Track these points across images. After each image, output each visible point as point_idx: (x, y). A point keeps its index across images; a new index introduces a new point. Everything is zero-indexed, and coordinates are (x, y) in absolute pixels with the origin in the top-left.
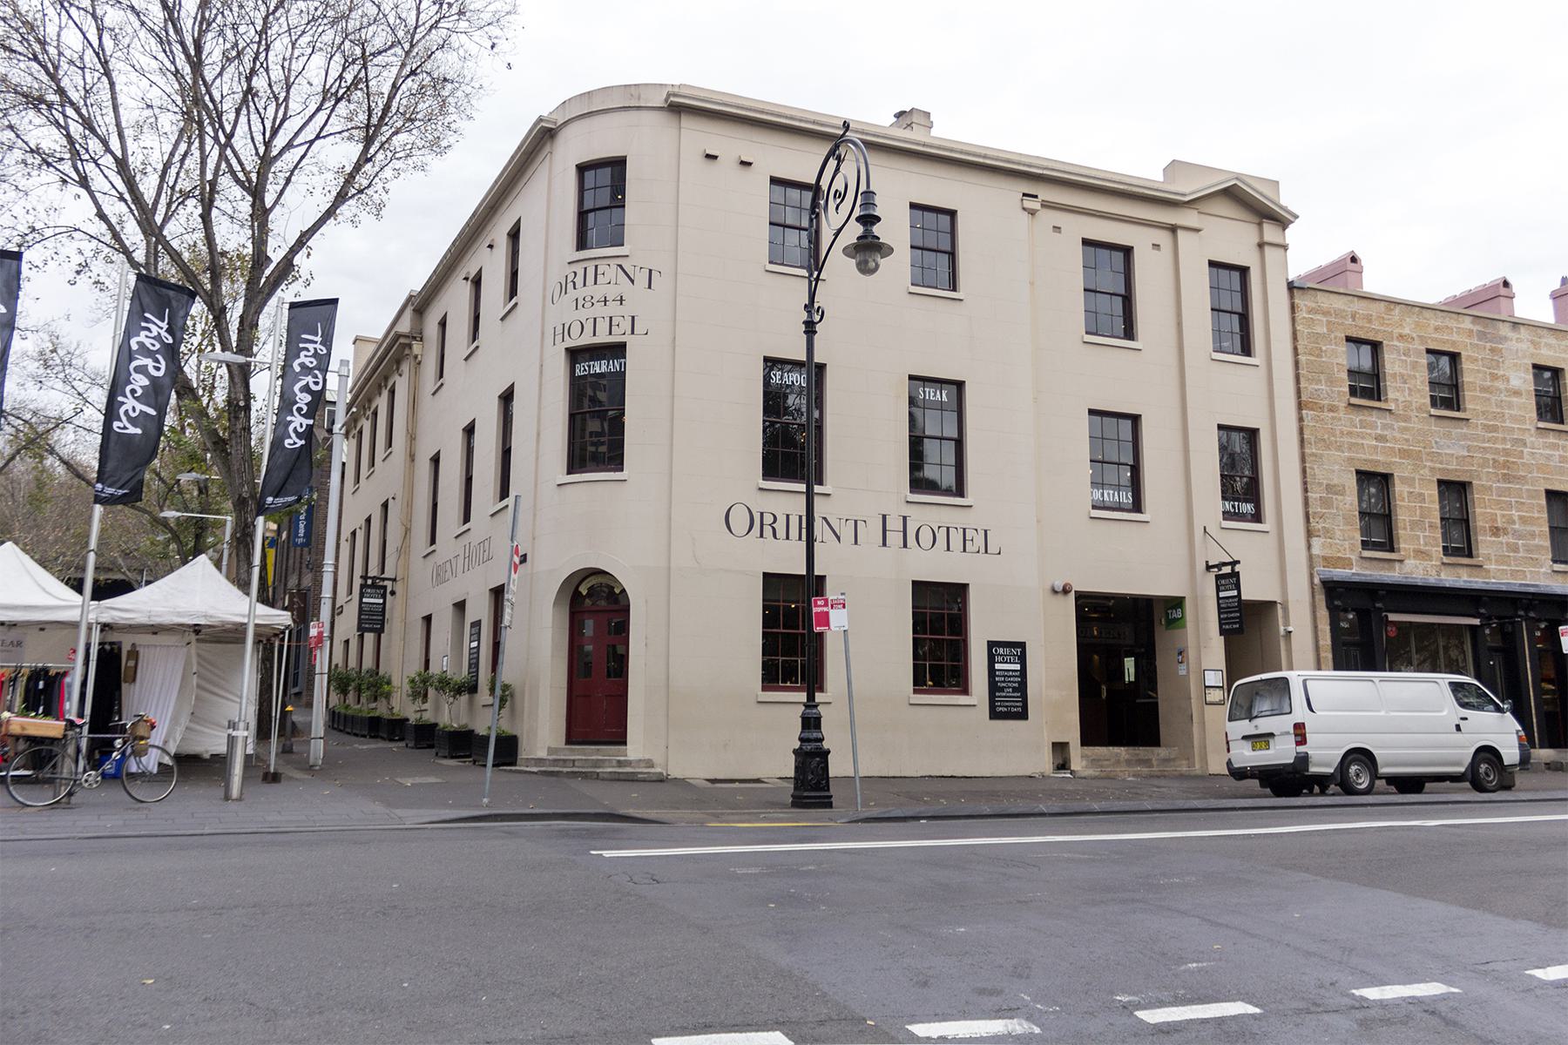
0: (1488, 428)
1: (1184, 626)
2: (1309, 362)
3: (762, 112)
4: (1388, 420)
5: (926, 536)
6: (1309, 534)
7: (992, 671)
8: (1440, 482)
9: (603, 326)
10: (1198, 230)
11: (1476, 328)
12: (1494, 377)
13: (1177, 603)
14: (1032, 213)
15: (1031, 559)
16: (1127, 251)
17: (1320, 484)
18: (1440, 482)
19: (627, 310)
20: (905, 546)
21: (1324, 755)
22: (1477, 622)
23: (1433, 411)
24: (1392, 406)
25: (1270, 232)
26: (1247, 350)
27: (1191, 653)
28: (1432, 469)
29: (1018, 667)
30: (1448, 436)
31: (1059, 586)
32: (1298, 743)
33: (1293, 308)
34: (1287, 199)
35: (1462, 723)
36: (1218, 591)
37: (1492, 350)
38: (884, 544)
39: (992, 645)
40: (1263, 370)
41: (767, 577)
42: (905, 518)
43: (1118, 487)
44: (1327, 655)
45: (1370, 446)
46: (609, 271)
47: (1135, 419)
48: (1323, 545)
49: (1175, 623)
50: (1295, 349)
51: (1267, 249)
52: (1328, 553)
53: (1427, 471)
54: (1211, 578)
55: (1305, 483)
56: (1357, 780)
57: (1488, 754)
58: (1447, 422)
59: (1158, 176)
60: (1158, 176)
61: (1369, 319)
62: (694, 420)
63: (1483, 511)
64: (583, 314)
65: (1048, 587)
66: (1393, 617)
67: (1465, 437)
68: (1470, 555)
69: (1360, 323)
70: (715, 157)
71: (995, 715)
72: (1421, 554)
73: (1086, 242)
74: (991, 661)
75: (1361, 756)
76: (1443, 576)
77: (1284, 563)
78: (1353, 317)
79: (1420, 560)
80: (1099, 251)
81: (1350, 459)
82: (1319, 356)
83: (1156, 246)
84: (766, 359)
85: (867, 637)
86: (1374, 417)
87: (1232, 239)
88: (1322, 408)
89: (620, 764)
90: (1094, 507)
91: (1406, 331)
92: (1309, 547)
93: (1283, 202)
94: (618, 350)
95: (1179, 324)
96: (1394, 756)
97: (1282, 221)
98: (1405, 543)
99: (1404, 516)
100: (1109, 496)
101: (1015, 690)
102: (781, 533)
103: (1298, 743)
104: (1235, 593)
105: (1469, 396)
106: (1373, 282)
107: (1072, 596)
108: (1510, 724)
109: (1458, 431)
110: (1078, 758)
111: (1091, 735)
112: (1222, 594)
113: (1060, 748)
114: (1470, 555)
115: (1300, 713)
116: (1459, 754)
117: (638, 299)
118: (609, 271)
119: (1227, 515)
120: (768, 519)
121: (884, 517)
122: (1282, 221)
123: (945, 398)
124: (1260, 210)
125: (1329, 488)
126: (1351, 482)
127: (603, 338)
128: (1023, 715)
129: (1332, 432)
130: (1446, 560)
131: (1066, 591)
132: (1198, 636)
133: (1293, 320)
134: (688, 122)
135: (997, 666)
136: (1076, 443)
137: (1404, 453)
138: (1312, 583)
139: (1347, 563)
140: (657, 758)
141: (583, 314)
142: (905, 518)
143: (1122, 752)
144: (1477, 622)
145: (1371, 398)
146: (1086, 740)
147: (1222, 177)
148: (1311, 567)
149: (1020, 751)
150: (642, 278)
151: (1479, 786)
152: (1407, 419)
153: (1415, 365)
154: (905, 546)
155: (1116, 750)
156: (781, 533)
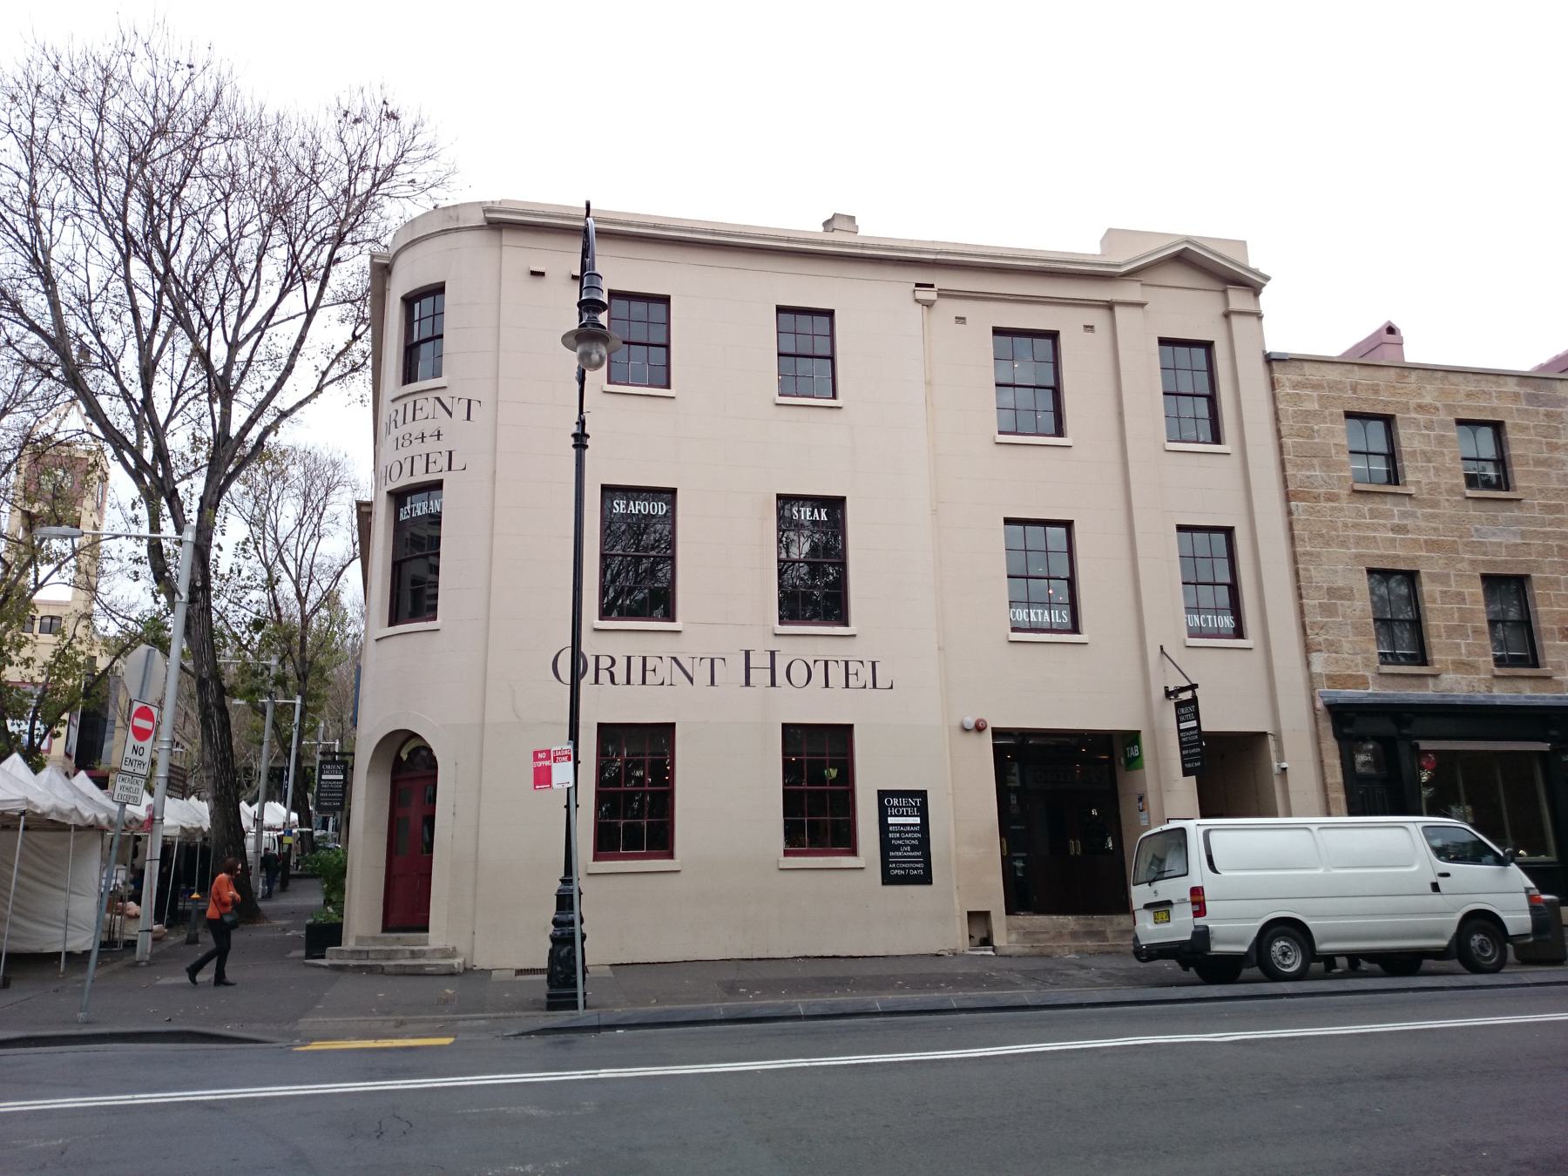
0: (1548, 508)
1: (1141, 767)
2: (1295, 445)
3: (664, 228)
4: (1408, 506)
5: (799, 673)
6: (1308, 649)
7: (884, 826)
8: (1485, 577)
9: (420, 465)
10: (1142, 305)
11: (1522, 391)
12: (1553, 447)
13: (1132, 737)
14: (929, 305)
15: (932, 692)
16: (1054, 336)
17: (1319, 588)
18: (1485, 577)
19: (444, 446)
20: (773, 684)
21: (1232, 928)
22: (1546, 747)
23: (1469, 493)
24: (1412, 490)
25: (1238, 299)
26: (1217, 438)
27: (1151, 799)
28: (1472, 562)
29: (917, 820)
30: (1493, 521)
31: (970, 722)
32: (1197, 914)
33: (1273, 384)
34: (1257, 260)
35: (1442, 881)
36: (1179, 722)
37: (1548, 415)
38: (748, 683)
39: (882, 794)
40: (1235, 460)
41: (600, 725)
42: (773, 653)
43: (1217, 611)
44: (1339, 796)
45: (1386, 539)
46: (428, 405)
47: (1068, 525)
48: (1326, 660)
49: (1134, 763)
50: (1278, 431)
51: (1234, 319)
52: (1334, 670)
53: (1465, 565)
54: (1171, 705)
55: (1299, 588)
56: (1283, 959)
57: (1481, 921)
58: (1490, 505)
59: (1098, 251)
60: (1098, 251)
61: (1375, 390)
62: (518, 557)
63: (1547, 610)
64: (404, 453)
65: (957, 723)
66: (1425, 745)
67: (1518, 522)
68: (1536, 665)
69: (1363, 395)
70: (542, 274)
71: (888, 879)
72: (1461, 666)
73: (997, 331)
74: (883, 813)
75: (1290, 929)
76: (1496, 692)
77: (1265, 688)
78: (1354, 390)
79: (1463, 671)
80: (1016, 339)
81: (1358, 557)
82: (1310, 437)
83: (1089, 328)
84: (779, 497)
85: (728, 792)
86: (1388, 505)
87: (1190, 311)
88: (1316, 498)
89: (414, 954)
90: (1014, 630)
91: (1427, 400)
92: (1308, 664)
93: (1252, 264)
94: (438, 485)
95: (1121, 414)
96: (1333, 926)
97: (1252, 285)
98: (1439, 655)
99: (1435, 623)
100: (1039, 616)
101: (914, 848)
102: (620, 676)
103: (1197, 914)
104: (1194, 724)
105: (1520, 475)
106: (1415, 352)
107: (988, 734)
108: (1517, 877)
109: (1506, 514)
110: (1004, 932)
111: (1019, 898)
112: (1183, 726)
113: (978, 918)
114: (1536, 665)
115: (1198, 873)
116: (1437, 921)
117: (457, 433)
118: (428, 405)
119: (1195, 633)
120: (605, 663)
121: (747, 653)
122: (1252, 285)
123: (824, 517)
124: (1230, 279)
125: (1332, 592)
126: (1362, 583)
127: (420, 477)
128: (926, 878)
129: (1332, 525)
130: (1498, 672)
131: (979, 728)
132: (1159, 781)
133: (1274, 398)
134: (509, 238)
135: (891, 820)
136: (991, 554)
137: (1432, 545)
138: (1314, 708)
139: (1362, 682)
140: (463, 947)
141: (404, 453)
142: (773, 653)
143: (1070, 922)
144: (1546, 747)
145: (1498, 487)
146: (1010, 911)
147: (1167, 242)
148: (1312, 689)
149: (925, 923)
150: (460, 410)
151: (1473, 966)
152: (1434, 504)
153: (1441, 440)
154: (773, 684)
155: (1062, 919)
156: (620, 676)
